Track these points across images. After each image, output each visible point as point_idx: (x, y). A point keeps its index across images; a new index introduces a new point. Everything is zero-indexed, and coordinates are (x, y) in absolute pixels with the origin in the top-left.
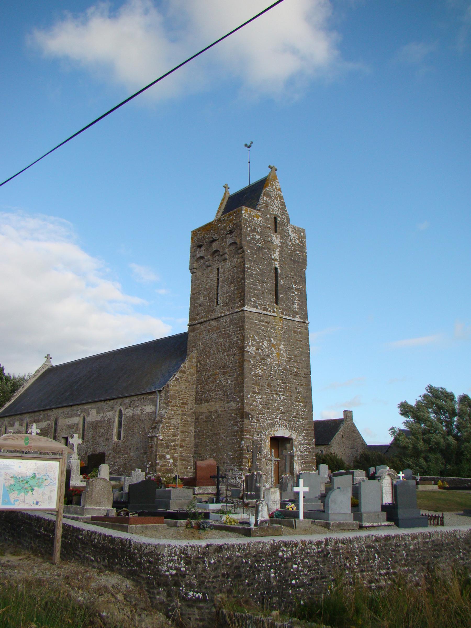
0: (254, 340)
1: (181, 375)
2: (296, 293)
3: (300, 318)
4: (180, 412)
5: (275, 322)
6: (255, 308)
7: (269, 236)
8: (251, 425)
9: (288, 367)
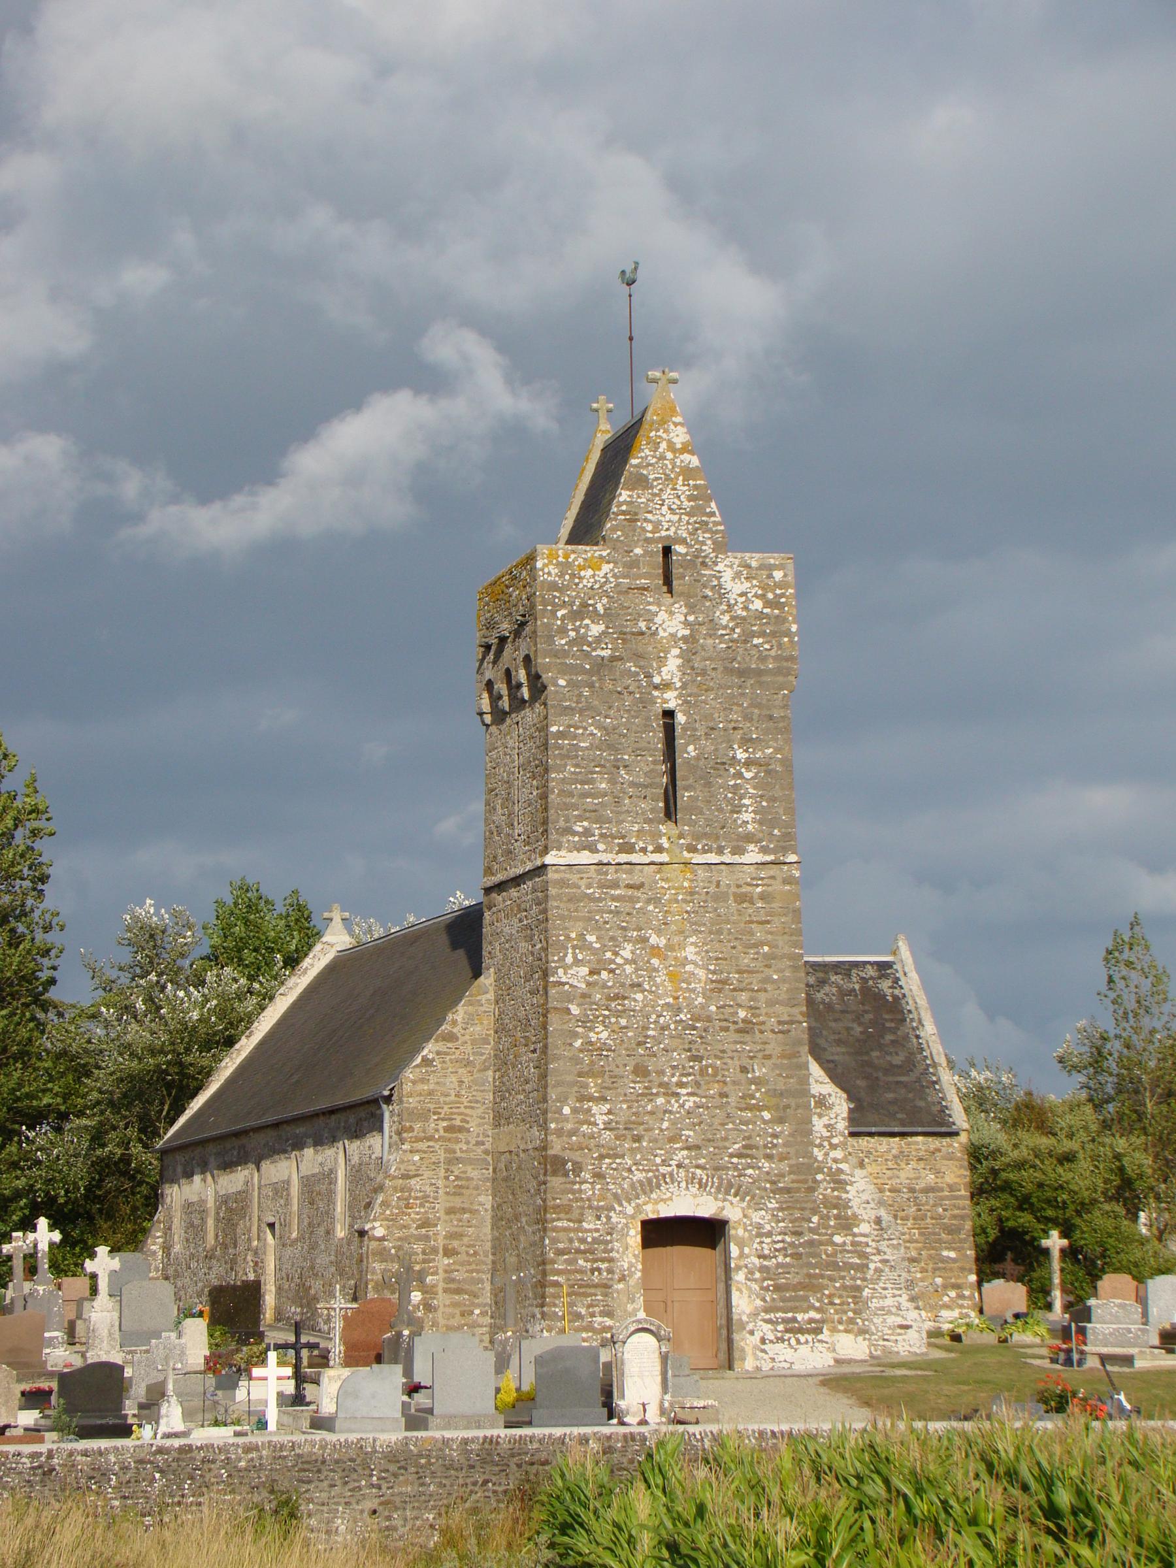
0: (585, 946)
1: (441, 1046)
2: (748, 775)
3: (764, 850)
4: (442, 1155)
5: (663, 880)
6: (586, 852)
7: (640, 616)
8: (573, 1192)
9: (713, 1008)
